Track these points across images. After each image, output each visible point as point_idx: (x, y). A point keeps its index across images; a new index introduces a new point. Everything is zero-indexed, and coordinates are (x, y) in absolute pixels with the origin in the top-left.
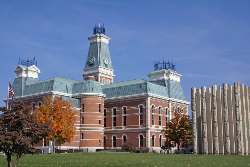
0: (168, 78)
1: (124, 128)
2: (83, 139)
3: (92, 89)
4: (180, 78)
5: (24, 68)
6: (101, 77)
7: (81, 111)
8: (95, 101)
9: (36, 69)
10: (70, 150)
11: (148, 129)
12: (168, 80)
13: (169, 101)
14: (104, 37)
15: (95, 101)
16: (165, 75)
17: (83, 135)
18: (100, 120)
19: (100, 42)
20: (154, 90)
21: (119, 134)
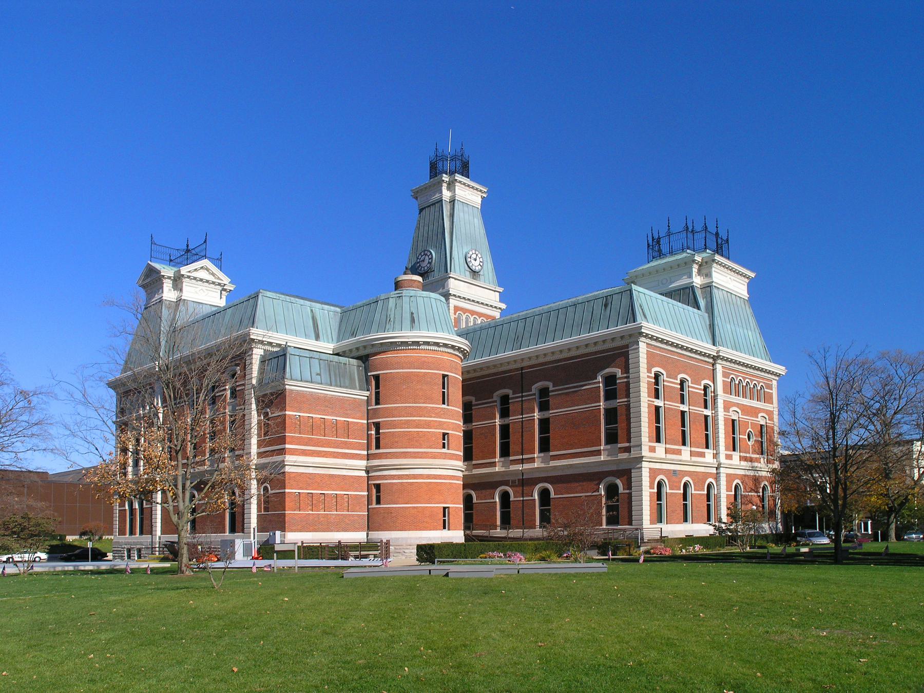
0: (707, 281)
1: (538, 462)
2: (378, 502)
3: (413, 321)
4: (748, 284)
5: (167, 271)
6: (457, 309)
7: (368, 402)
8: (423, 364)
9: (213, 274)
10: (304, 547)
11: (640, 459)
12: (708, 288)
13: (715, 358)
14: (464, 184)
15: (423, 364)
16: (695, 268)
17: (378, 491)
18: (444, 435)
19: (453, 201)
20: (659, 317)
21: (525, 482)
